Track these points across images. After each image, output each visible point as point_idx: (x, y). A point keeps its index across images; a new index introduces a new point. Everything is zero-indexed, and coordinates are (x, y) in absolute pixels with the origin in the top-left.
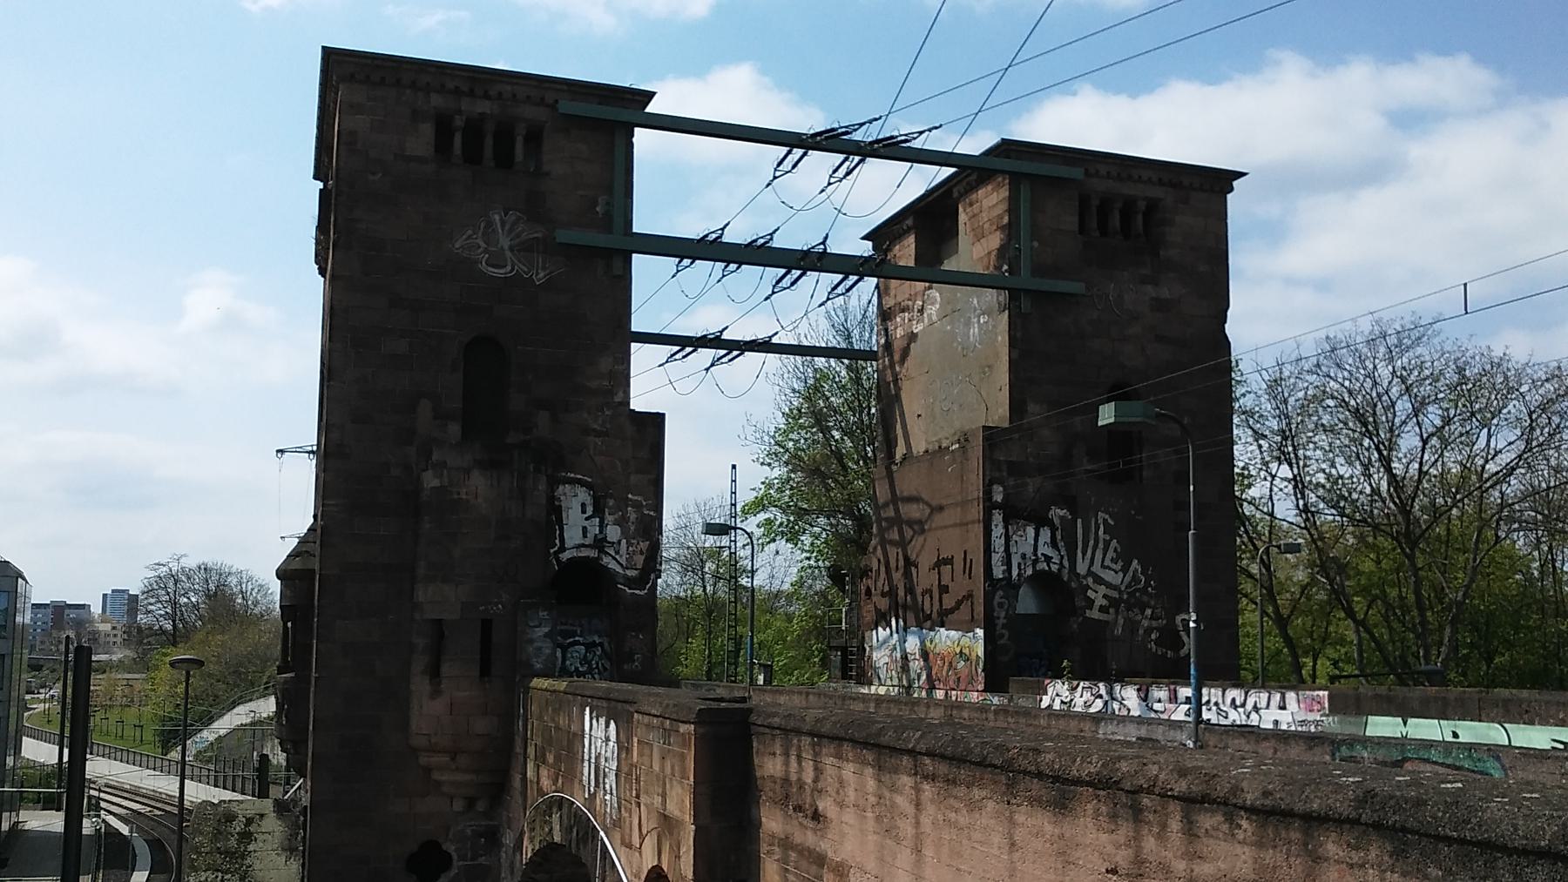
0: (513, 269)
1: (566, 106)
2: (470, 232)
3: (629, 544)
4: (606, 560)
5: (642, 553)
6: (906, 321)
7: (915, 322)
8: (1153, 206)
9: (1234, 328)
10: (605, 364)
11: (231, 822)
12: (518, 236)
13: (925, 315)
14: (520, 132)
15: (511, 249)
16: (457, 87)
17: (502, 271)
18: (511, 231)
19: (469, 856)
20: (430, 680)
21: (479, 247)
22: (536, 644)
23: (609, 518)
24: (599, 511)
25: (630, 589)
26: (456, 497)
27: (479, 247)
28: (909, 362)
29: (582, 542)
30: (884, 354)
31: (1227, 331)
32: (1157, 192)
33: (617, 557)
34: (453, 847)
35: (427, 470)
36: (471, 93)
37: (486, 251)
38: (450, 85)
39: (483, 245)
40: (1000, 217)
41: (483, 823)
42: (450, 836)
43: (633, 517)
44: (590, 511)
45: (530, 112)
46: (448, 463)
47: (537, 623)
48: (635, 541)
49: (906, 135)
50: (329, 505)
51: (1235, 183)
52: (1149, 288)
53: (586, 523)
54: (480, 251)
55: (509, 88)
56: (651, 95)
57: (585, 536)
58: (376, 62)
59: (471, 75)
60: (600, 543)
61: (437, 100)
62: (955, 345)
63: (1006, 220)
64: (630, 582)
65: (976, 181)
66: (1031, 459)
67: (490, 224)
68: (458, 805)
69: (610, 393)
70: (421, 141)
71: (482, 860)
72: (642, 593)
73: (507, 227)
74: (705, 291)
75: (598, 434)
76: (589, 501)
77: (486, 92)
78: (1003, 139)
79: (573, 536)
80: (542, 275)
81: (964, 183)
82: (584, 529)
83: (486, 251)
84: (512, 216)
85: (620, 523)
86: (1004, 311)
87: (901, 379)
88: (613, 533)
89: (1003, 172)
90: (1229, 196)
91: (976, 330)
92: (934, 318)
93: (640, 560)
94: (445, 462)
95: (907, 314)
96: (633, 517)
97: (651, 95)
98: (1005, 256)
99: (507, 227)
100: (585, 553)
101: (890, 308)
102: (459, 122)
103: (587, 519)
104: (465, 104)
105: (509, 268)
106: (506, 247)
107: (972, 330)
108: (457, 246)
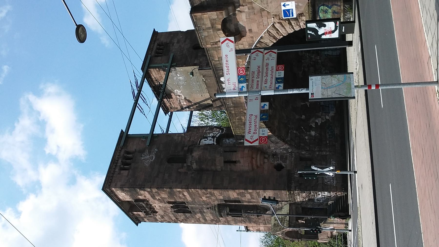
0: (154, 155)
1: (122, 144)
2: (145, 163)
3: (214, 132)
4: (217, 136)
5: (216, 129)
6: (182, 101)
7: (182, 98)
8: (158, 45)
9: (184, 30)
10: (176, 138)
11: (275, 224)
12: (147, 154)
13: (180, 95)
14: (126, 155)
15: (149, 155)
16: (115, 166)
17: (154, 157)
18: (146, 155)
19: (278, 159)
20: (236, 163)
21: (148, 161)
22: (230, 142)
23: (208, 136)
24: (207, 138)
25: (224, 131)
26: (198, 159)
27: (148, 161)
28: (191, 100)
29: (213, 141)
30: (190, 109)
31: (185, 31)
32: (156, 44)
33: (217, 134)
34: (276, 162)
35: (192, 167)
36: (117, 163)
37: (149, 160)
38: (114, 167)
39: (148, 160)
40: (157, 71)
41: (271, 156)
42: (273, 163)
43: (208, 131)
44: (206, 139)
45: (122, 153)
46: (190, 161)
47: (226, 142)
48: (214, 131)
49: (162, 131)
50: (198, 187)
51: (156, 31)
52: (174, 44)
53: (209, 140)
54: (149, 161)
55: (116, 156)
56: (122, 131)
57: (211, 140)
58: (107, 180)
59: (113, 163)
60: (213, 137)
61: (117, 170)
62: (185, 84)
63: (157, 69)
64: (222, 132)
65: (150, 79)
66: (206, 62)
67: (144, 159)
68: (266, 160)
69: (182, 136)
70: (125, 173)
71: (279, 157)
72: (225, 129)
73: (145, 156)
74: (110, 17)
75: (190, 138)
76: (204, 139)
77: (117, 160)
78: (141, 69)
79: (211, 142)
80: (156, 150)
81: (151, 82)
82: (210, 140)
83: (149, 160)
84: (143, 156)
85: (209, 133)
86: (175, 69)
87: (195, 102)
88: (211, 135)
89: (147, 69)
90: (159, 32)
91: (181, 77)
92: (180, 91)
93: (218, 130)
94: (191, 161)
95: (181, 101)
96: (208, 131)
97: (122, 131)
98: (164, 69)
99: (145, 156)
100: (215, 140)
101: (180, 107)
102: (122, 166)
103: (208, 140)
104: (119, 165)
105: (153, 156)
106: (149, 156)
107: (181, 79)
108: (147, 165)
